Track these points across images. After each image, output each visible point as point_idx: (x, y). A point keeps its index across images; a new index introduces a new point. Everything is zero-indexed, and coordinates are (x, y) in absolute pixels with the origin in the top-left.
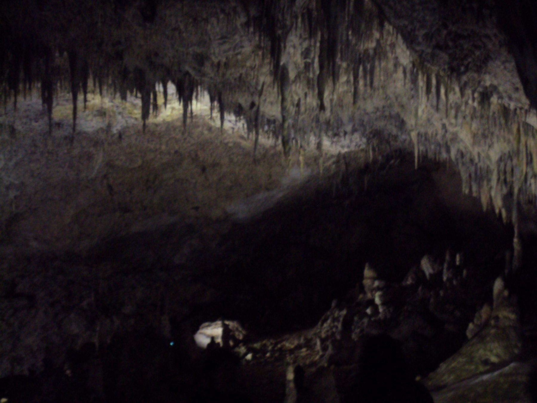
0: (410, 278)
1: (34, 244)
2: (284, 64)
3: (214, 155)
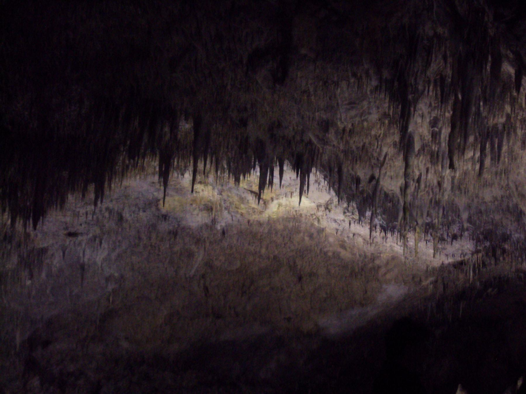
1: (125, 344)
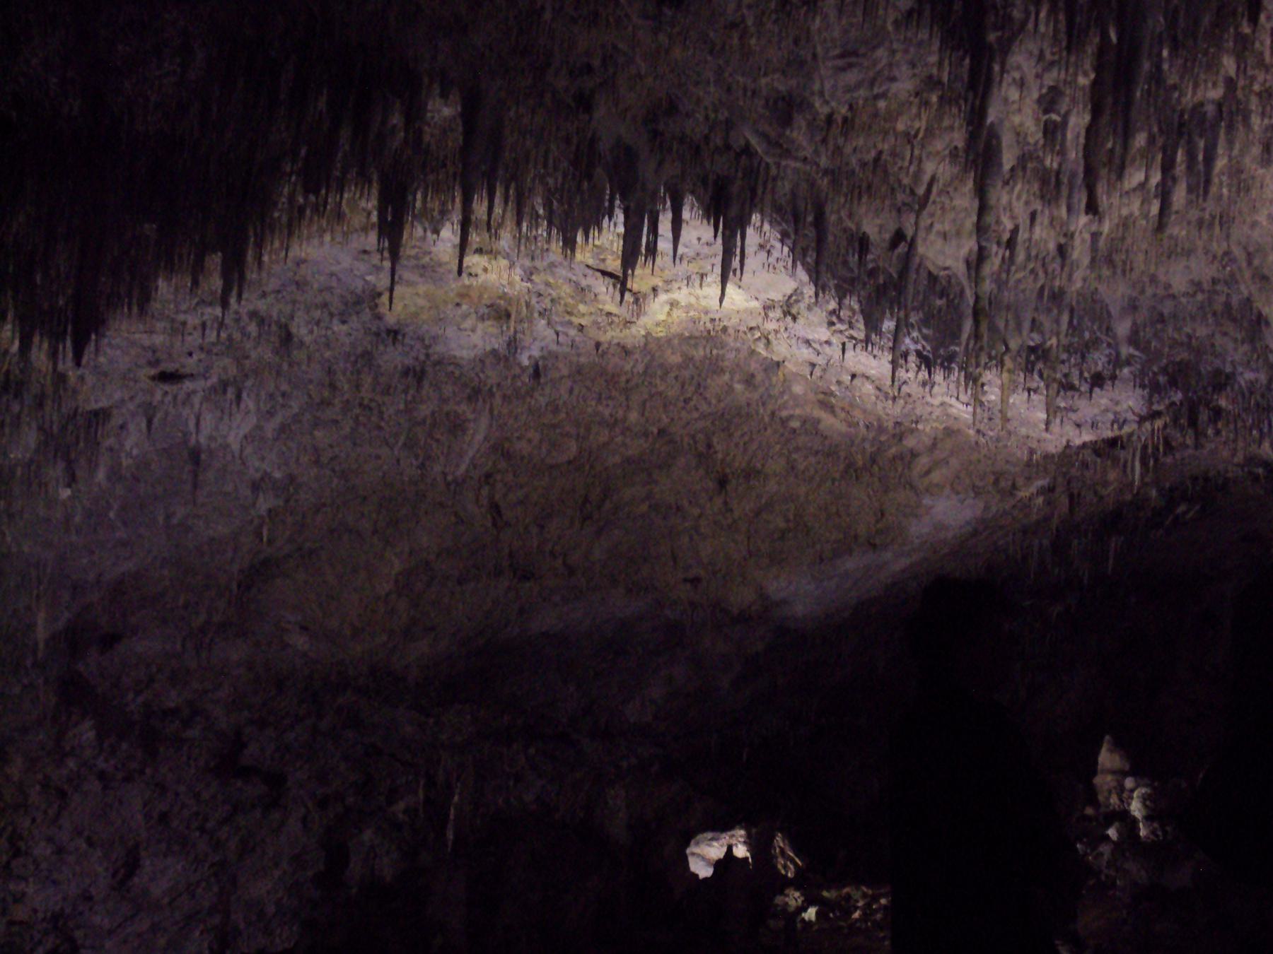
1: (300, 642)
2: (992, 124)
3: (754, 447)
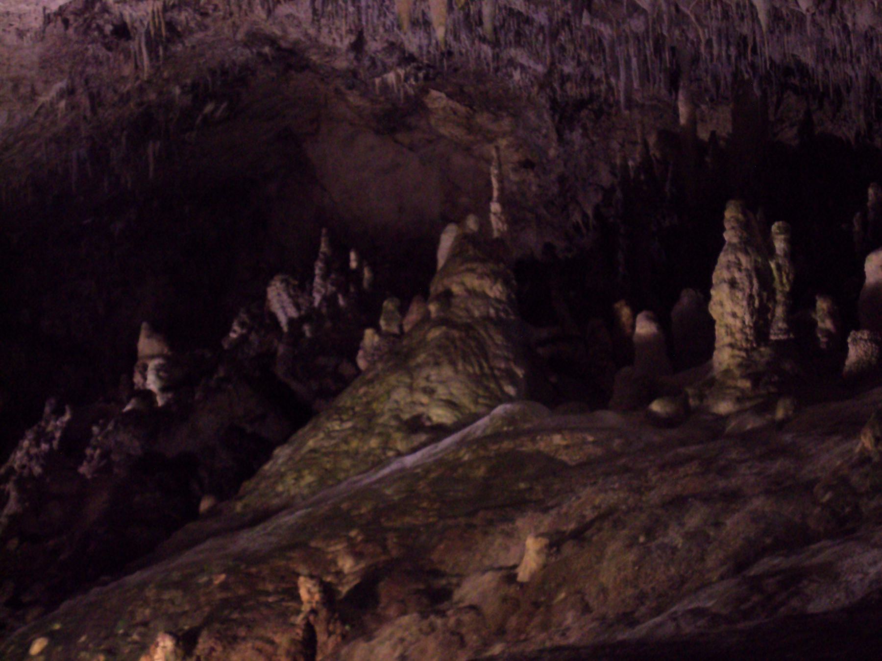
0: (236, 327)
